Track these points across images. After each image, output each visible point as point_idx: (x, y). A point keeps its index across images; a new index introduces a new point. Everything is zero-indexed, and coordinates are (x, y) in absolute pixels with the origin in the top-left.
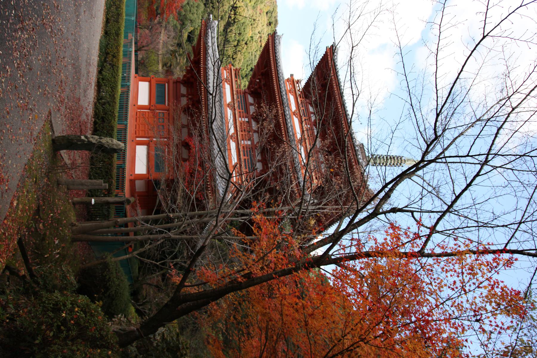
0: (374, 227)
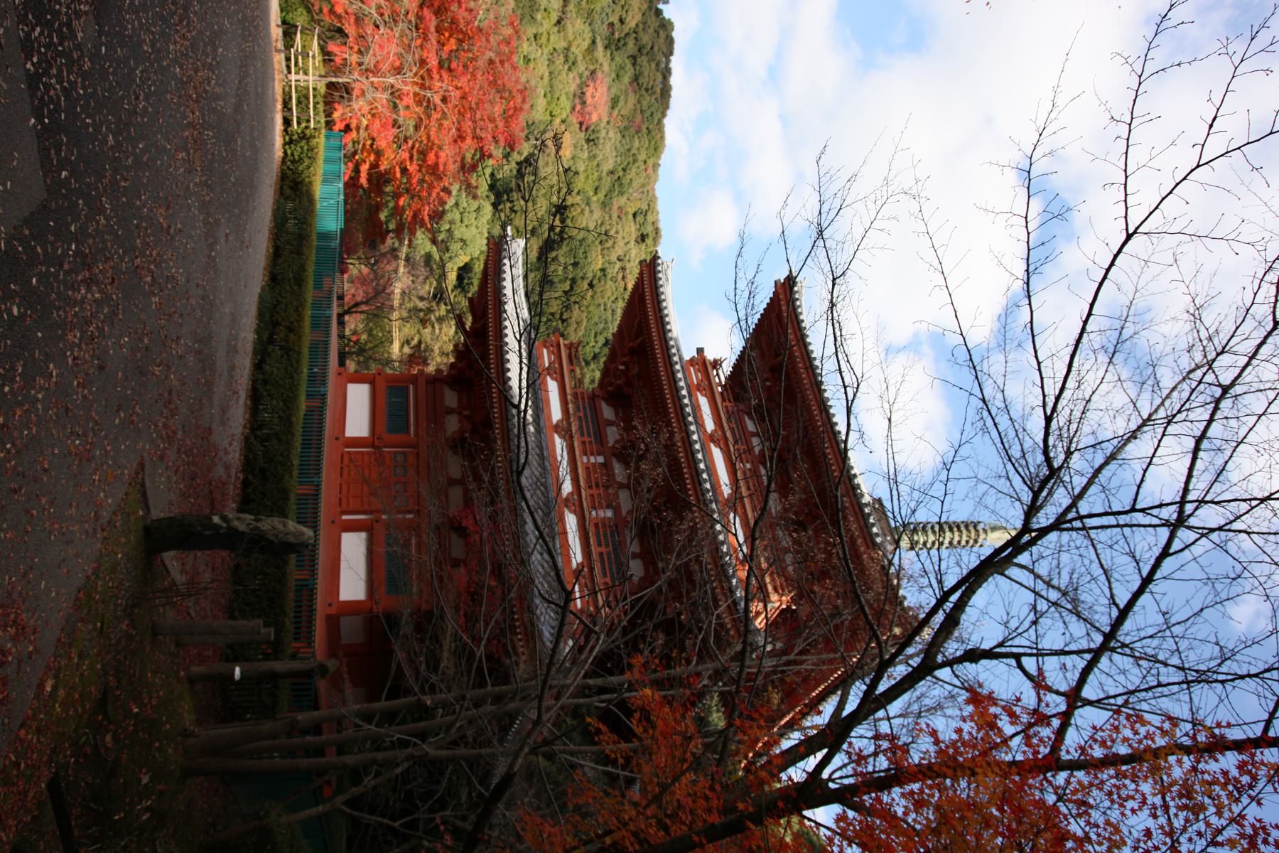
0: (927, 701)
